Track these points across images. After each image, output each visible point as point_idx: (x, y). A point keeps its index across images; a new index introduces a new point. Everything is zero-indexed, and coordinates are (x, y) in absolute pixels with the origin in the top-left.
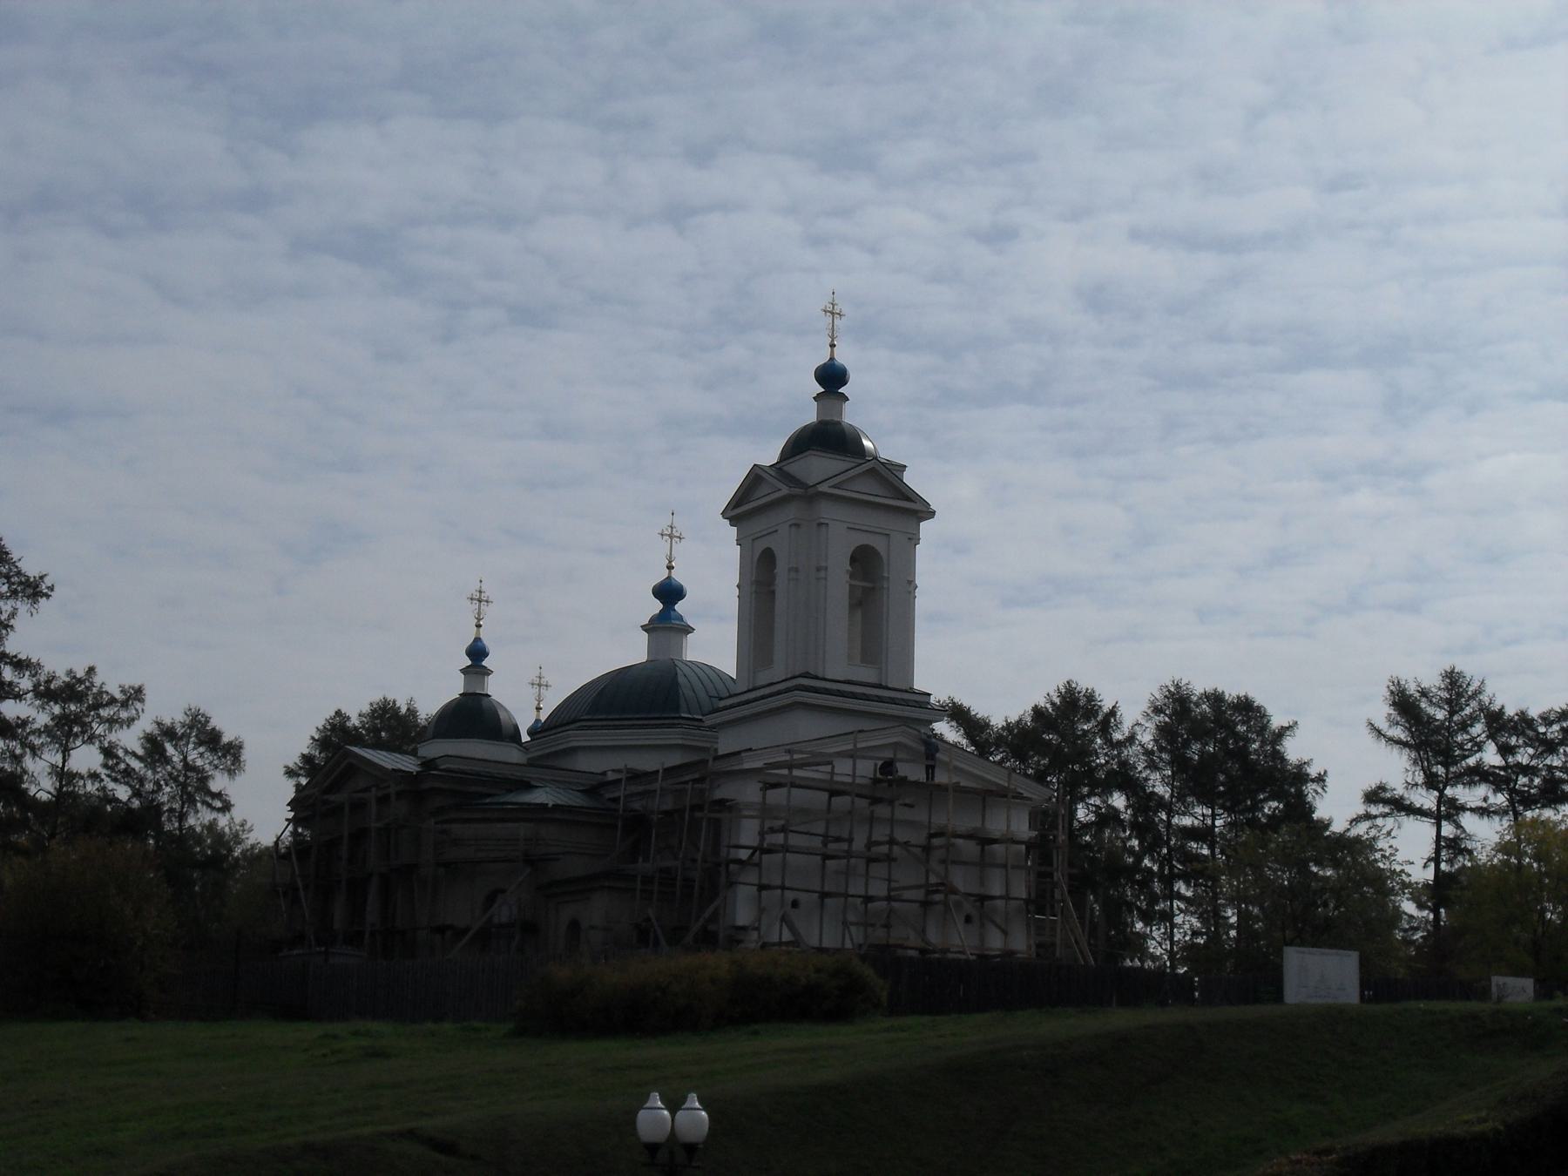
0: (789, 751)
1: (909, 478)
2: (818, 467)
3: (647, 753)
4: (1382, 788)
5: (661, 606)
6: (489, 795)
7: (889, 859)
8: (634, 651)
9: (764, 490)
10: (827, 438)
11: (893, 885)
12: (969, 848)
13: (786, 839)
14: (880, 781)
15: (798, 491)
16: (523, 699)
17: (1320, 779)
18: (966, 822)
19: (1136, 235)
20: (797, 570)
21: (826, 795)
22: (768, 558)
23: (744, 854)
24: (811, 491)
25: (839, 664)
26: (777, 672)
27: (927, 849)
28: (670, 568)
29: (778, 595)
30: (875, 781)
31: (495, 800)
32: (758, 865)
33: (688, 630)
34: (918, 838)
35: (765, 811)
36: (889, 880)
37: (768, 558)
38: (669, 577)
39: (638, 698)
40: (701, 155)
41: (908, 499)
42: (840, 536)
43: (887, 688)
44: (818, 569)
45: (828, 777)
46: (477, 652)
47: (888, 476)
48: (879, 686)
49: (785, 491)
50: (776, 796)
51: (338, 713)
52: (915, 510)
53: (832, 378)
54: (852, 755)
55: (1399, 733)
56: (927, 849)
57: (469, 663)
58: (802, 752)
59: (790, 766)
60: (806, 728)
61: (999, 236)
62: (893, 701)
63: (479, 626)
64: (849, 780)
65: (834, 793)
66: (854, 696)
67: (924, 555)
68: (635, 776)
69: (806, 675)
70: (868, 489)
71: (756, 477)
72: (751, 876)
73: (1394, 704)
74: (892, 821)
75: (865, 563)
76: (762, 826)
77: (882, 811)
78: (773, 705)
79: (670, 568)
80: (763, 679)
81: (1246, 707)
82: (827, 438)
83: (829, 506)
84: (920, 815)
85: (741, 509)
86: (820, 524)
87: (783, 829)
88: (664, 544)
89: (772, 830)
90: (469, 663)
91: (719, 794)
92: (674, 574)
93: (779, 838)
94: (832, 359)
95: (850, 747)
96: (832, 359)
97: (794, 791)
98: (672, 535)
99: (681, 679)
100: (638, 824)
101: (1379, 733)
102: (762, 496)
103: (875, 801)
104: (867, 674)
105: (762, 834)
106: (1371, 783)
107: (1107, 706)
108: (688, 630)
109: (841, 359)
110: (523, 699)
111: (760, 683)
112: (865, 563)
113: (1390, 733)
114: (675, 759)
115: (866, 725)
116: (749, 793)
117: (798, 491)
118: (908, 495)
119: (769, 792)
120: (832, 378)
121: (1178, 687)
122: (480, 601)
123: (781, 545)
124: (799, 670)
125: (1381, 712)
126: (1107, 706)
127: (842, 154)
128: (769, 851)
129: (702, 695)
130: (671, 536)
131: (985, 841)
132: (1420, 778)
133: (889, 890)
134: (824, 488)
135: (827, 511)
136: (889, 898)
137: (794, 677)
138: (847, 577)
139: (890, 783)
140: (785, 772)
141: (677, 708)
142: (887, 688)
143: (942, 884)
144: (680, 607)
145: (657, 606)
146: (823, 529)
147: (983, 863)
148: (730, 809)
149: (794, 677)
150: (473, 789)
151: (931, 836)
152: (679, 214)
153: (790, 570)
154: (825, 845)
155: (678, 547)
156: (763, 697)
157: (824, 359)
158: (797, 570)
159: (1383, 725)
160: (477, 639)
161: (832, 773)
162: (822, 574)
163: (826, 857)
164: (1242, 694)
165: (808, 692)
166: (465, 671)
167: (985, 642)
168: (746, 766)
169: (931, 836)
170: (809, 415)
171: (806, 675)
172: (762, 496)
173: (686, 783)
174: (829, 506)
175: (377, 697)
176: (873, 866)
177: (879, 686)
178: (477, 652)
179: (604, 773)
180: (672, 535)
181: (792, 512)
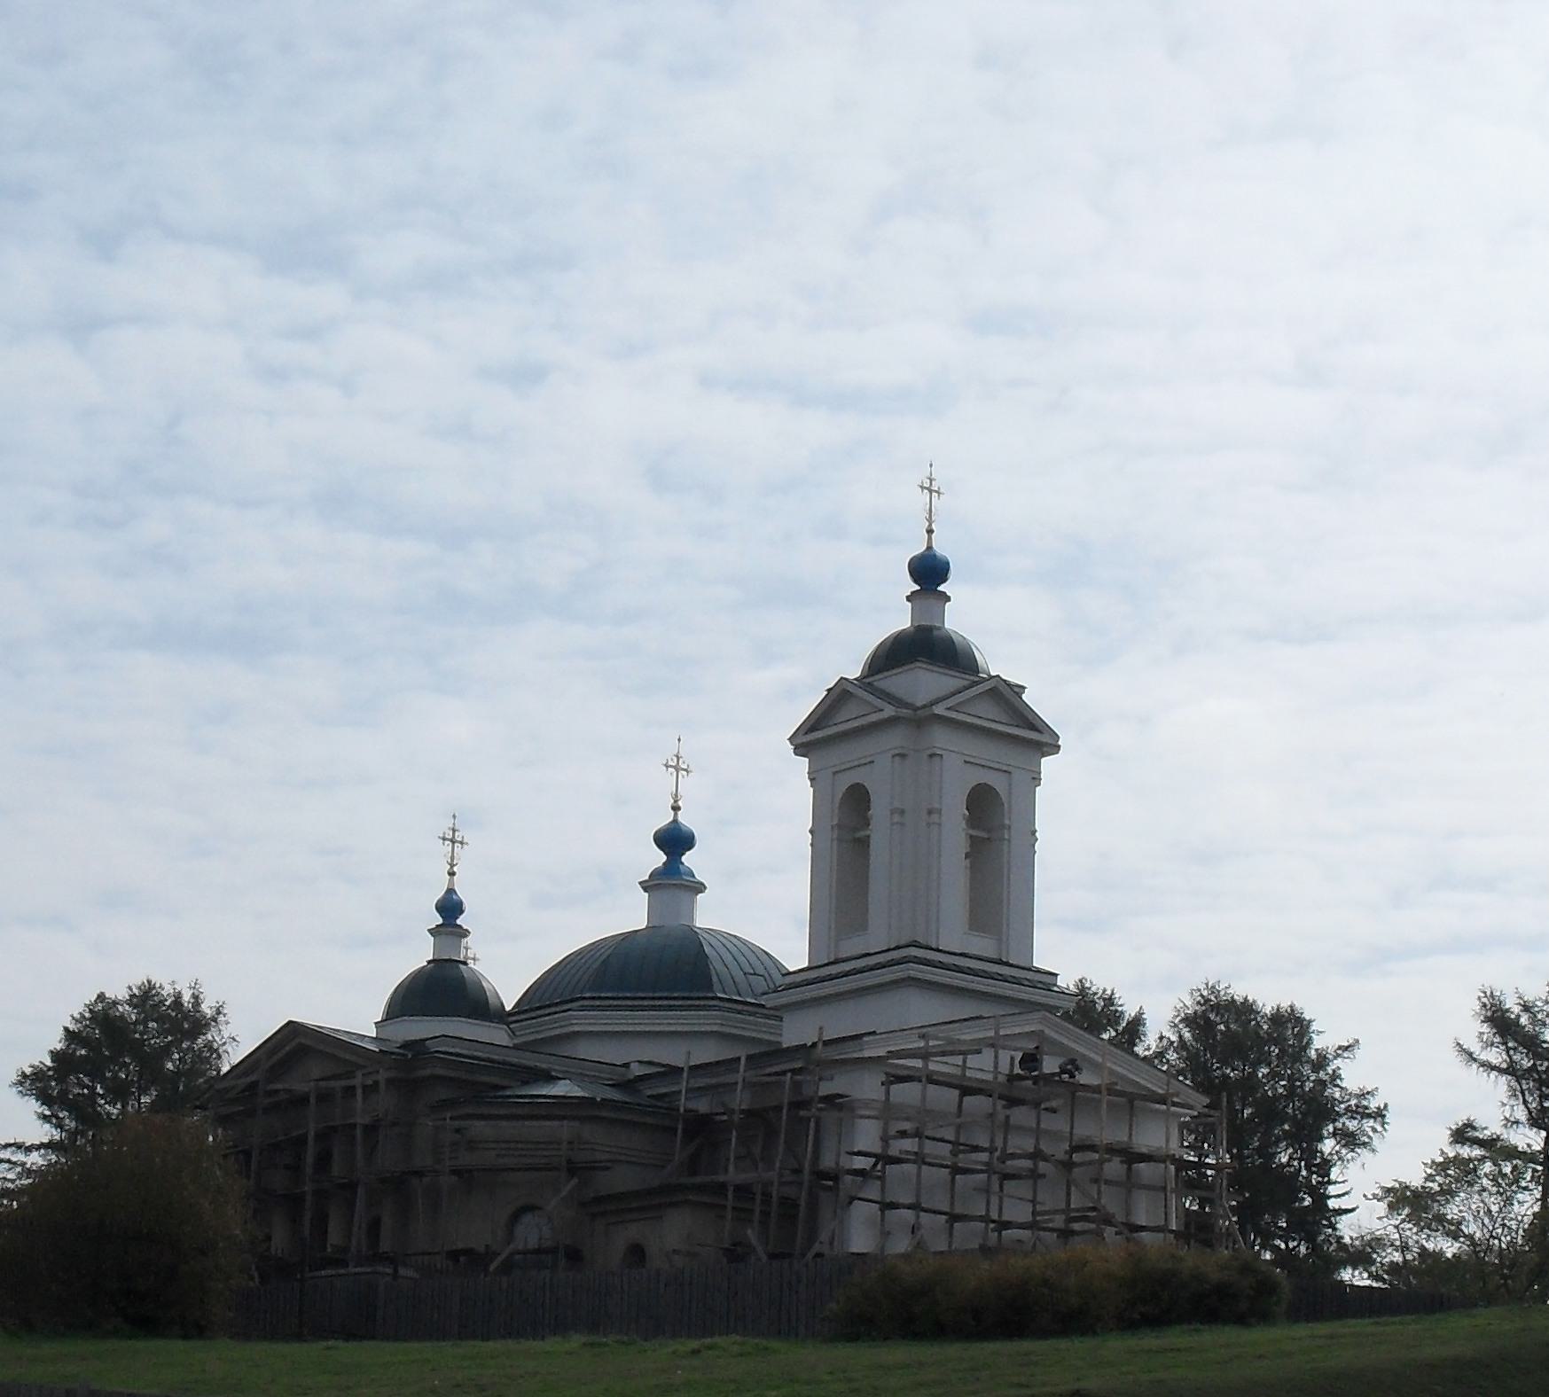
0: (923, 1037)
2: (923, 683)
4: (1469, 1125)
5: (665, 858)
6: (504, 1088)
7: (1034, 1175)
8: (630, 914)
9: (844, 714)
10: (924, 647)
11: (1039, 1208)
12: (1114, 1168)
13: (921, 1146)
14: (1020, 1078)
16: (507, 969)
17: (1380, 1115)
18: (1114, 1134)
19: (707, 381)
21: (956, 1092)
22: (857, 799)
23: (861, 1163)
24: (926, 712)
26: (877, 937)
27: (1068, 1165)
28: (676, 808)
30: (1012, 1078)
31: (508, 1093)
32: (882, 1178)
34: (1059, 1150)
35: (887, 1111)
36: (1034, 1202)
37: (857, 799)
38: (675, 821)
39: (661, 968)
40: (104, 243)
41: (1037, 730)
42: (957, 768)
43: (1007, 964)
44: (930, 812)
45: (958, 1072)
46: (450, 908)
47: (1006, 696)
48: (1000, 962)
49: (889, 711)
50: (906, 1093)
51: (101, 997)
52: (1034, 738)
53: (929, 573)
54: (993, 1044)
55: (1496, 1056)
56: (1068, 1165)
57: (440, 921)
58: (937, 1039)
59: (925, 1055)
60: (922, 1010)
61: (525, 376)
62: (1018, 981)
63: (452, 874)
64: (990, 1077)
65: (966, 1091)
68: (672, 1072)
70: (987, 714)
71: (839, 695)
72: (872, 1191)
73: (1487, 1020)
74: (1038, 1133)
76: (885, 1130)
77: (1022, 1115)
78: (843, 988)
79: (676, 808)
81: (1290, 1026)
82: (924, 647)
83: (923, 736)
84: (1058, 1123)
87: (918, 1134)
89: (903, 1134)
90: (440, 921)
91: (826, 1089)
92: (680, 819)
93: (909, 1145)
94: (929, 548)
95: (992, 1034)
96: (929, 548)
97: (931, 1087)
98: (677, 767)
99: (707, 949)
100: (700, 1126)
101: (1471, 1057)
102: (849, 718)
103: (1012, 1102)
104: (981, 945)
105: (885, 1139)
106: (1459, 1119)
107: (1130, 1011)
109: (940, 549)
110: (507, 969)
113: (1484, 1056)
114: (706, 1053)
115: (986, 1009)
116: (867, 1087)
118: (1029, 720)
119: (894, 1088)
120: (929, 573)
121: (1213, 990)
122: (453, 841)
123: (881, 783)
125: (1473, 1031)
126: (1130, 1011)
127: (303, 249)
128: (898, 1161)
129: (739, 976)
130: (677, 768)
131: (1132, 1157)
132: (1521, 1114)
133: (1034, 1213)
134: (939, 710)
135: (941, 738)
136: (1032, 1226)
138: (964, 825)
139: (1036, 1080)
140: (918, 1063)
141: (710, 987)
142: (1007, 964)
143: (1094, 1209)
144: (688, 859)
145: (660, 858)
146: (937, 759)
147: (1130, 1184)
148: (840, 1107)
150: (485, 1079)
151: (1076, 1148)
152: (81, 326)
153: (892, 812)
154: (954, 1154)
156: (846, 974)
157: (920, 548)
158: (902, 812)
159: (1475, 1048)
160: (451, 891)
161: (964, 1067)
162: (935, 817)
163: (956, 1170)
164: (1285, 1005)
165: (912, 966)
167: (1130, 911)
168: (867, 1054)
169: (1076, 1148)
170: (901, 620)
172: (849, 718)
173: (784, 1073)
174: (923, 736)
175: (173, 979)
176: (1010, 1186)
177: (1000, 962)
178: (450, 908)
179: (626, 1065)
180: (677, 767)
181: (894, 739)
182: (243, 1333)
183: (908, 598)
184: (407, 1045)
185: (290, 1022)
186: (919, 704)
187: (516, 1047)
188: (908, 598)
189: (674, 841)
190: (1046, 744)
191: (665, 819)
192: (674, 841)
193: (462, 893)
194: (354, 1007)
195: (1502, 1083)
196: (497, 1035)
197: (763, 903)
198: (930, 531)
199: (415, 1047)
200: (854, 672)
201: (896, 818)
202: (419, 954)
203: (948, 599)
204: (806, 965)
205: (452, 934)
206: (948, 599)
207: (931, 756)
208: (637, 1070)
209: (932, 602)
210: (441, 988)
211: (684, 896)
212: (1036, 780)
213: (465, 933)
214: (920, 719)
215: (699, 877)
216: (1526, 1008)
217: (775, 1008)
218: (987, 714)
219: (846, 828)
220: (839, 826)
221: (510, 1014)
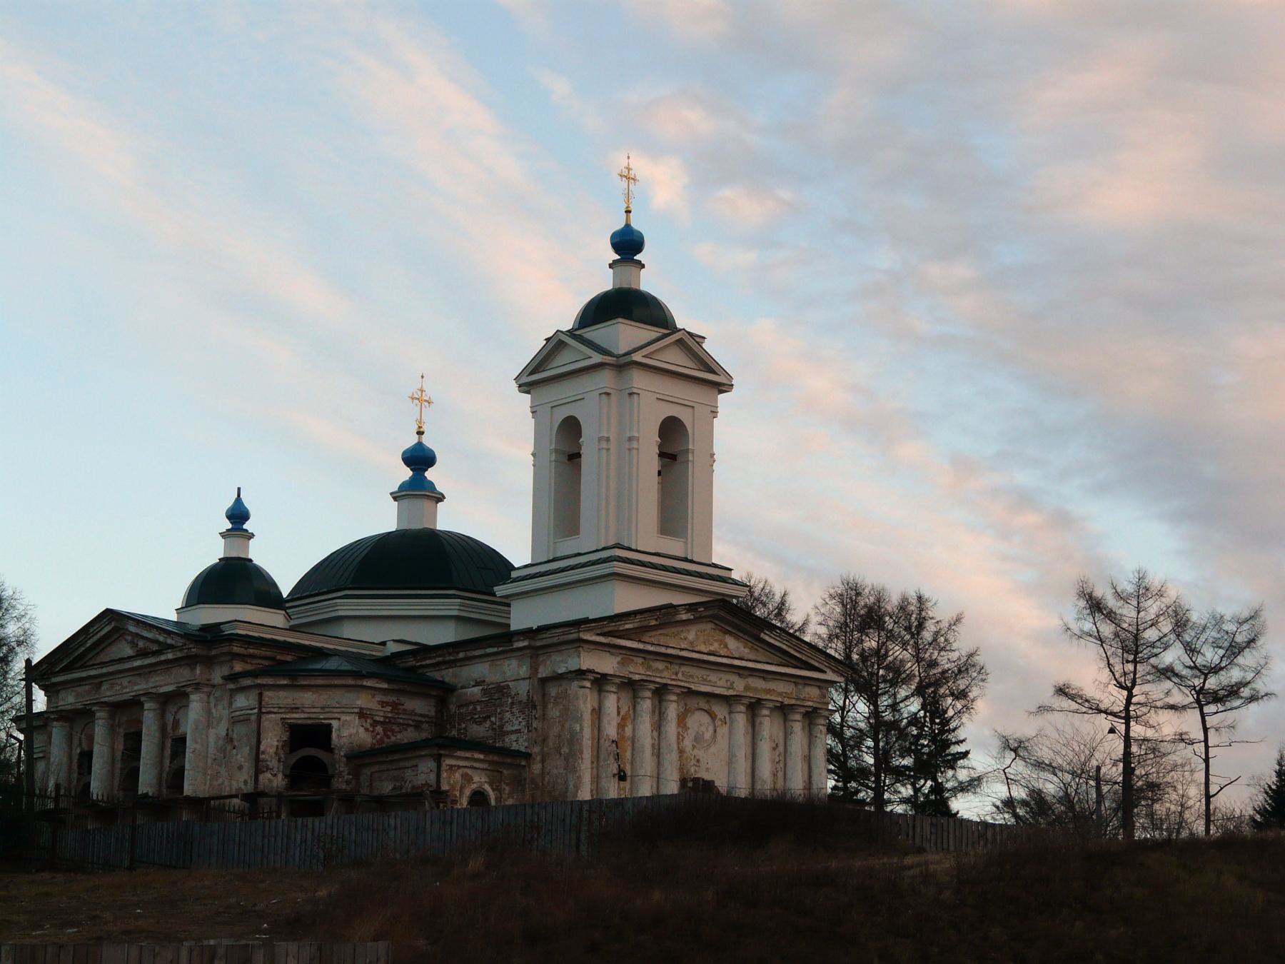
2: (624, 335)
3: (424, 622)
5: (411, 473)
8: (383, 519)
15: (608, 359)
16: (286, 559)
20: (608, 439)
22: (571, 428)
24: (626, 359)
25: (647, 538)
26: (588, 540)
29: (585, 460)
33: (440, 498)
37: (571, 428)
39: (415, 560)
42: (652, 402)
43: (692, 561)
47: (690, 344)
48: (686, 560)
49: (597, 358)
52: (710, 379)
53: (628, 245)
57: (230, 526)
66: (654, 566)
67: (720, 426)
69: (618, 546)
70: (675, 359)
71: (555, 345)
75: (671, 430)
79: (420, 433)
80: (569, 546)
82: (623, 304)
83: (623, 360)
85: (537, 377)
86: (631, 394)
88: (414, 409)
90: (230, 526)
98: (421, 400)
102: (564, 362)
104: (673, 546)
108: (440, 498)
110: (286, 559)
111: (559, 554)
112: (671, 430)
117: (608, 359)
118: (708, 365)
120: (628, 245)
124: (611, 543)
134: (637, 357)
135: (639, 380)
137: (604, 549)
142: (692, 561)
144: (430, 474)
145: (407, 473)
149: (604, 549)
155: (428, 413)
157: (620, 225)
158: (608, 439)
162: (635, 445)
165: (617, 563)
166: (223, 535)
170: (604, 282)
171: (618, 546)
172: (564, 362)
174: (623, 360)
177: (686, 560)
179: (383, 644)
181: (604, 379)
182: (139, 760)
183: (611, 266)
184: (206, 628)
185: (108, 615)
186: (621, 352)
187: (293, 629)
188: (611, 266)
189: (419, 459)
190: (724, 385)
191: (412, 440)
192: (419, 459)
193: (247, 502)
194: (160, 597)
195: (1093, 649)
196: (274, 618)
197: (494, 509)
198: (628, 212)
199: (211, 634)
200: (568, 325)
201: (604, 445)
202: (212, 552)
203: (643, 266)
204: (529, 562)
205: (243, 536)
206: (643, 266)
207: (631, 394)
208: (393, 648)
209: (630, 269)
210: (232, 579)
211: (427, 504)
212: (714, 413)
213: (252, 536)
214: (623, 365)
215: (439, 489)
216: (1118, 595)
217: (507, 597)
218: (675, 359)
219: (565, 449)
220: (556, 451)
221: (288, 601)
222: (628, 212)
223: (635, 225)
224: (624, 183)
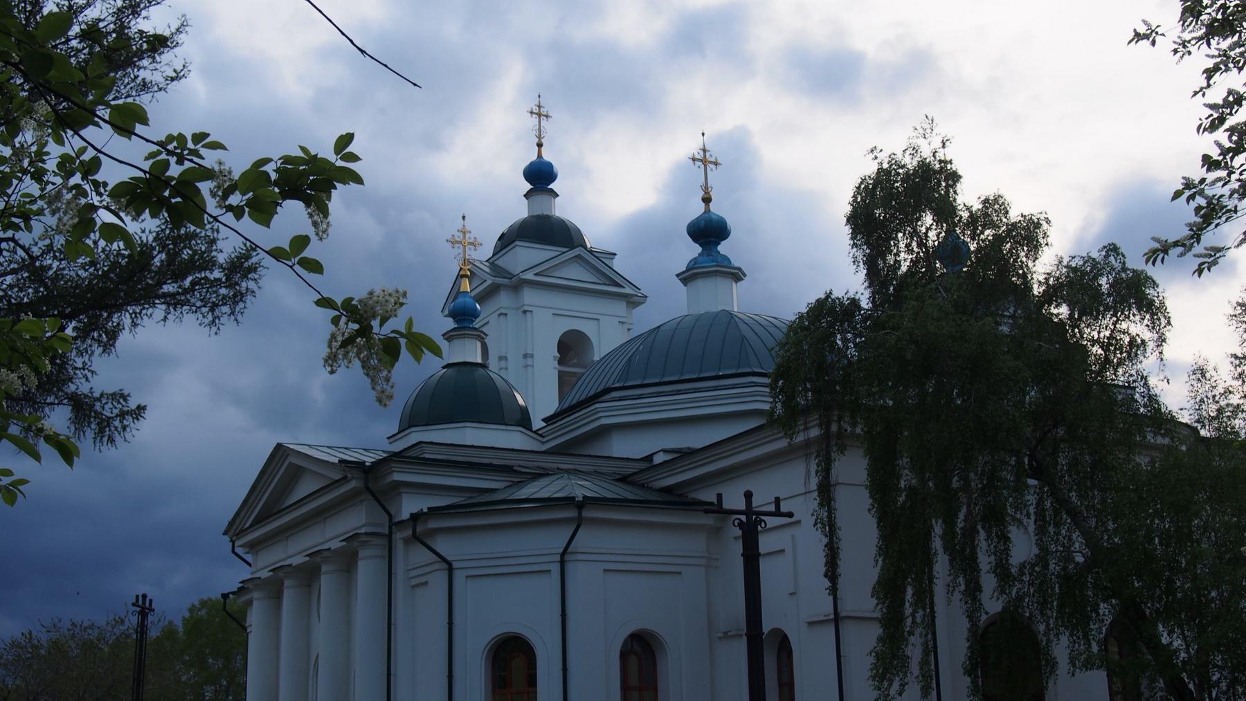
1: (617, 264)
70: (576, 274)
86: (525, 312)
134: (530, 276)
135: (530, 297)
145: (696, 249)
153: (501, 358)
162: (529, 361)
191: (697, 209)
198: (540, 145)
209: (540, 199)
222: (540, 145)
223: (547, 157)
224: (535, 119)
